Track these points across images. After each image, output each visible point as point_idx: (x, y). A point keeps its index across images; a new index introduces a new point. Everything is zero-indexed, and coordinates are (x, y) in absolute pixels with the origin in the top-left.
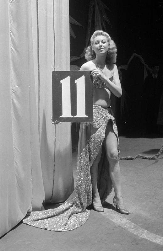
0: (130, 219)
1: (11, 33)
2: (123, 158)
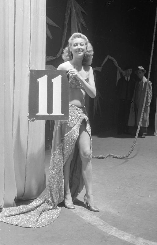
0: (100, 216)
2: (95, 156)
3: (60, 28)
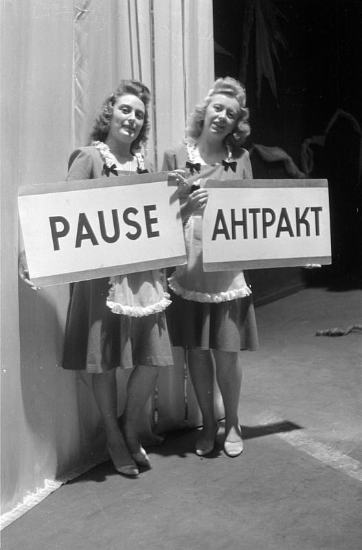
0: (349, 452)
1: (76, 79)
2: (322, 332)
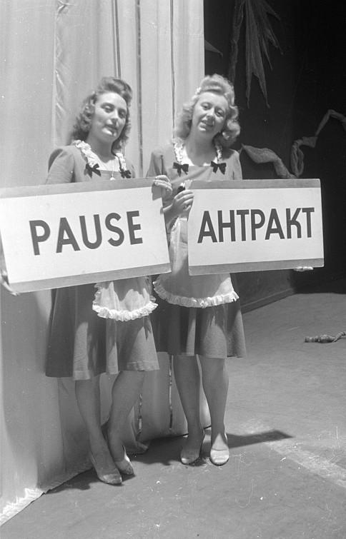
0: (338, 460)
1: (58, 75)
2: (311, 338)
3: (222, 54)
